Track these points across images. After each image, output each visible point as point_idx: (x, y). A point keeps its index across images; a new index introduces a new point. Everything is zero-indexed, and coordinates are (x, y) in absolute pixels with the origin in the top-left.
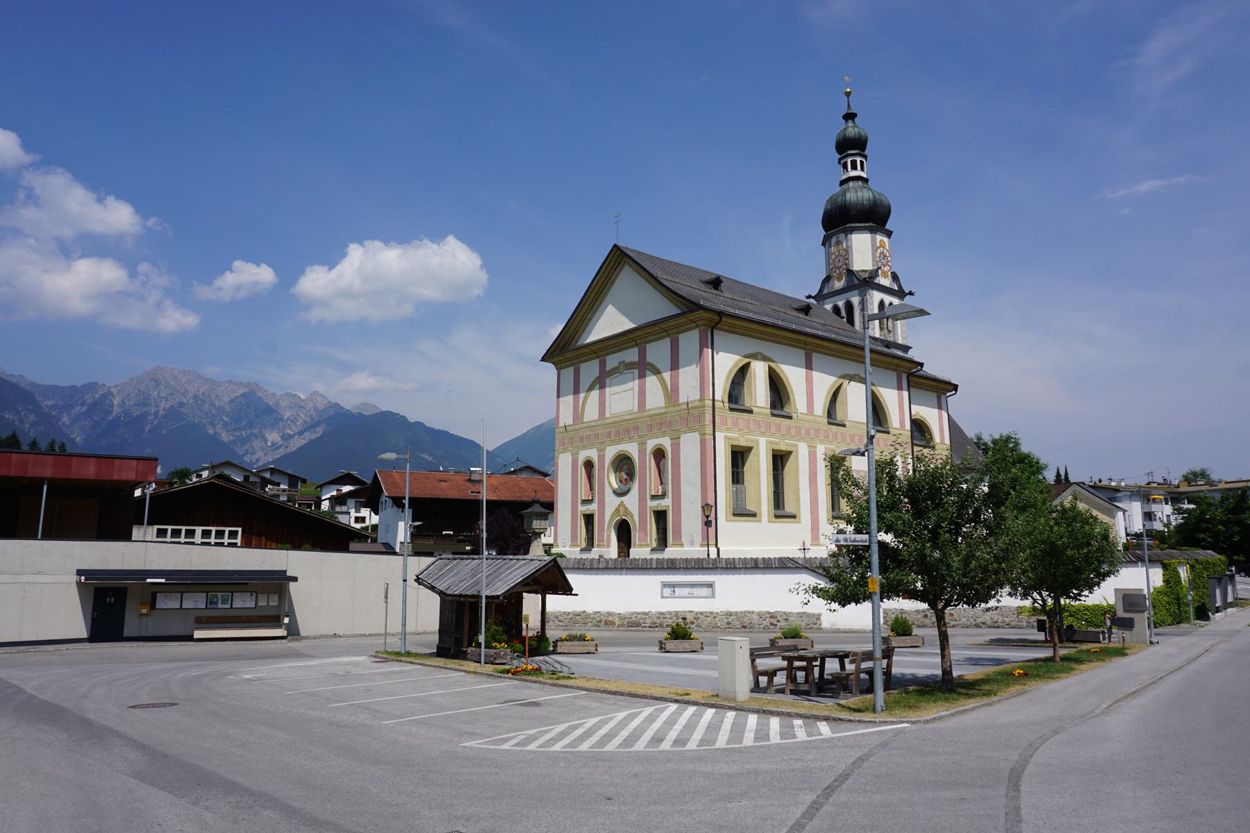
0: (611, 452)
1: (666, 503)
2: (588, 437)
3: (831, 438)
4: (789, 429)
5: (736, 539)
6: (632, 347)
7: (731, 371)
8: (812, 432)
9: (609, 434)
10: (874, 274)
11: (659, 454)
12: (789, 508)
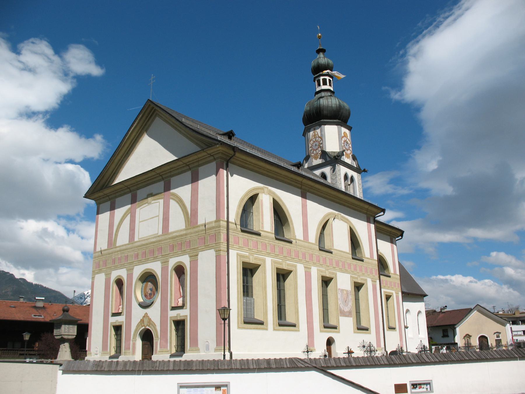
0: (138, 271)
1: (184, 313)
2: (120, 259)
3: (321, 262)
4: (289, 252)
5: (247, 344)
6: (159, 181)
7: (242, 199)
8: (307, 257)
9: (137, 256)
10: (341, 154)
11: (180, 270)
12: (290, 319)
